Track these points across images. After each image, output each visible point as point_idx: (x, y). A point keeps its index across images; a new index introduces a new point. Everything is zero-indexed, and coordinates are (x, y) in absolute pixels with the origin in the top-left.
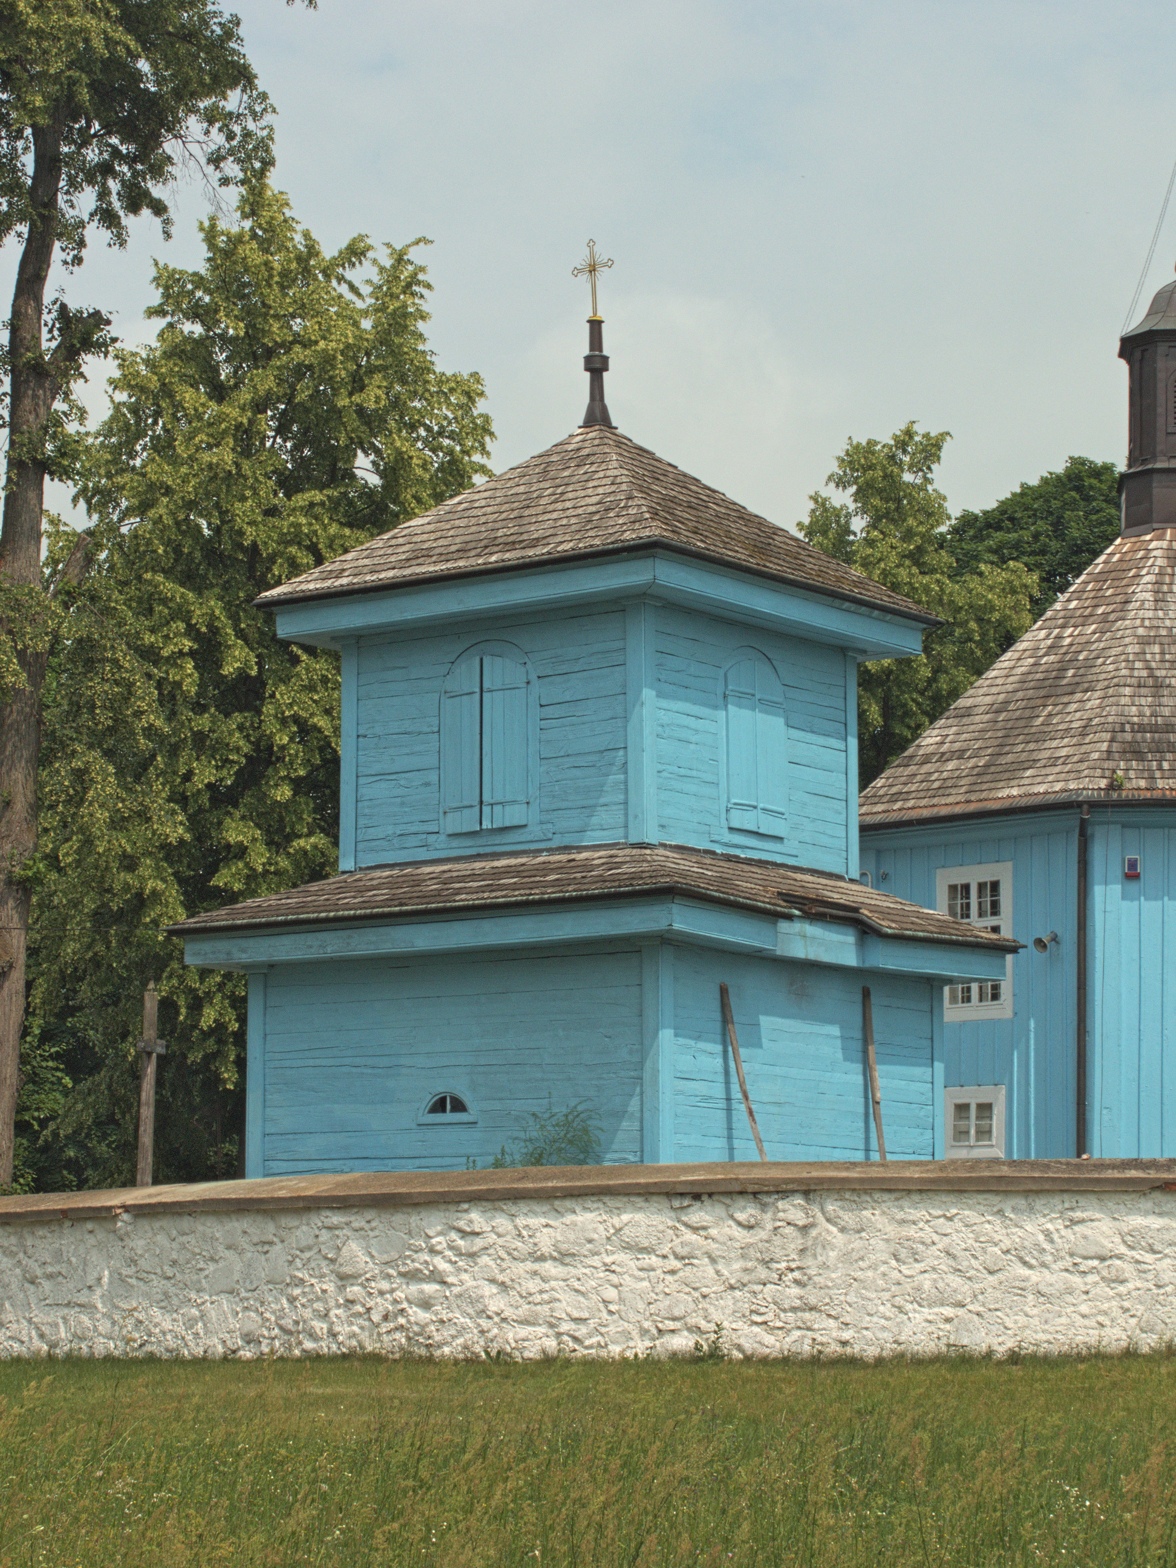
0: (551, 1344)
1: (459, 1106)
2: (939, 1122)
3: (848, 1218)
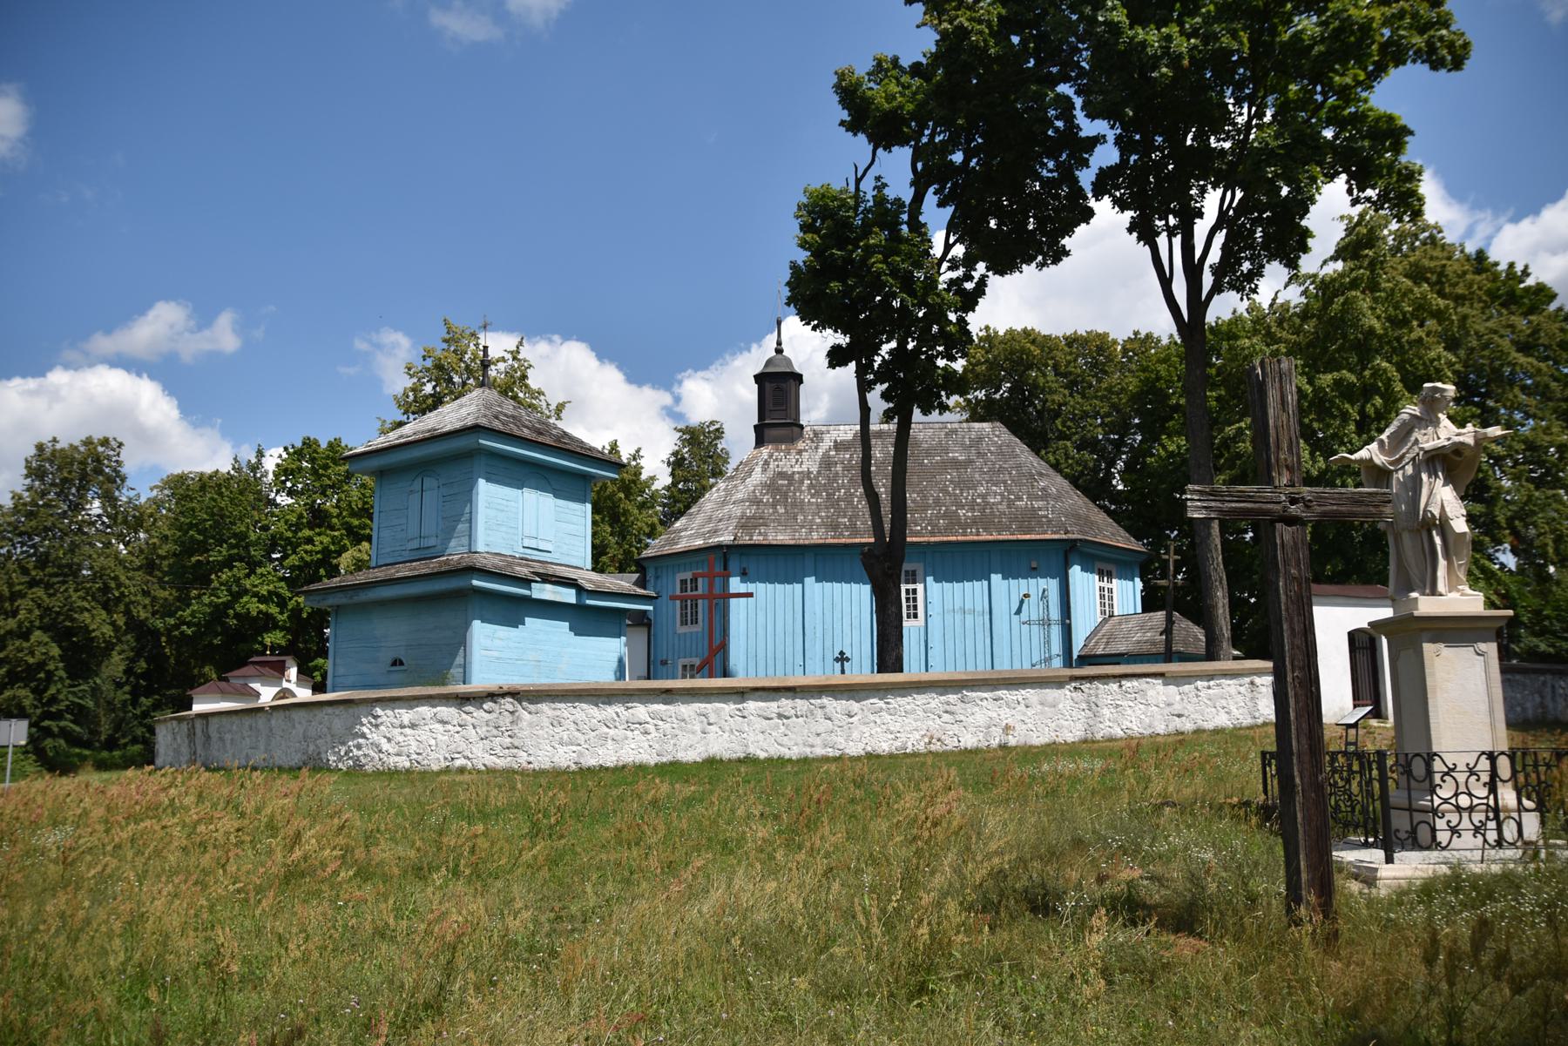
0: (407, 764)
1: (401, 663)
3: (532, 707)
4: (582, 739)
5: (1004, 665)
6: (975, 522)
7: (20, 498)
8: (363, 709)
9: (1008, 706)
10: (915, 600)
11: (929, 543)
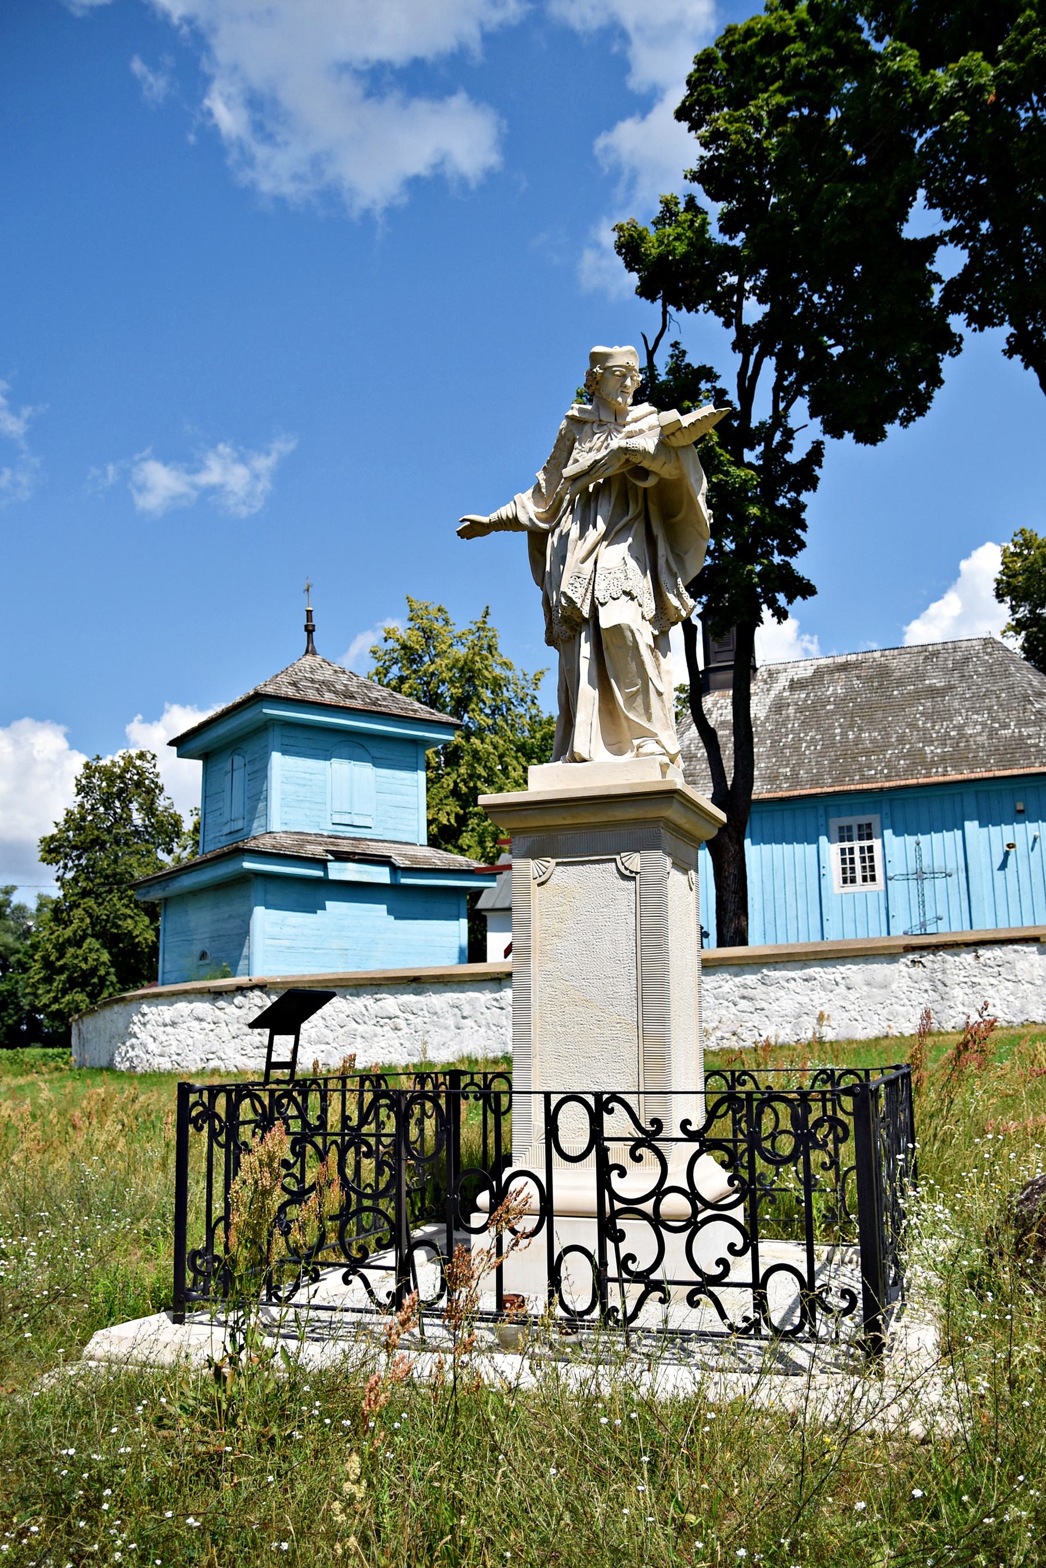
0: (169, 1066)
2: (538, 916)
4: (330, 1036)
5: (835, 935)
6: (943, 759)
7: (73, 813)
8: (133, 1006)
9: (823, 988)
10: (872, 859)
11: (881, 789)
